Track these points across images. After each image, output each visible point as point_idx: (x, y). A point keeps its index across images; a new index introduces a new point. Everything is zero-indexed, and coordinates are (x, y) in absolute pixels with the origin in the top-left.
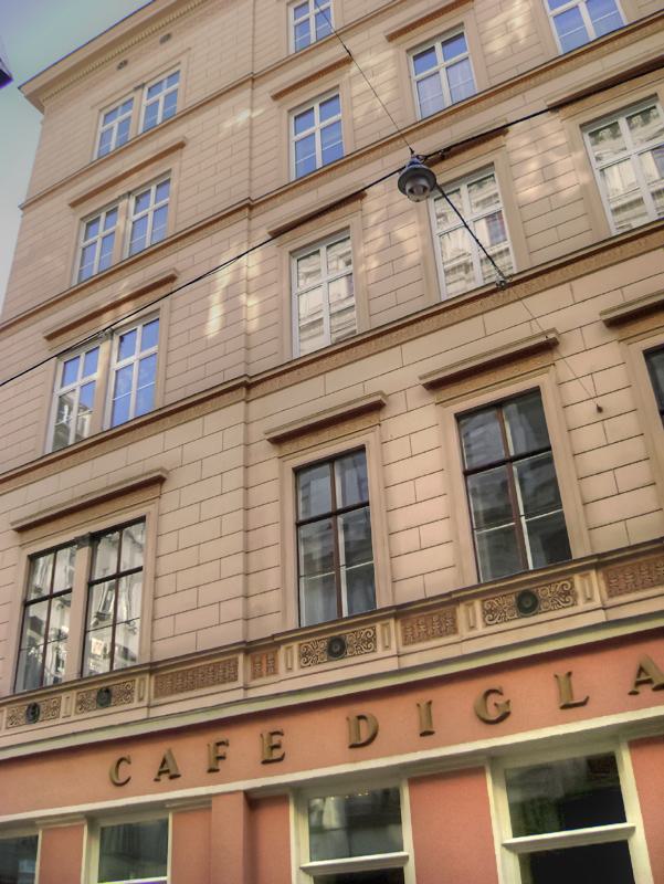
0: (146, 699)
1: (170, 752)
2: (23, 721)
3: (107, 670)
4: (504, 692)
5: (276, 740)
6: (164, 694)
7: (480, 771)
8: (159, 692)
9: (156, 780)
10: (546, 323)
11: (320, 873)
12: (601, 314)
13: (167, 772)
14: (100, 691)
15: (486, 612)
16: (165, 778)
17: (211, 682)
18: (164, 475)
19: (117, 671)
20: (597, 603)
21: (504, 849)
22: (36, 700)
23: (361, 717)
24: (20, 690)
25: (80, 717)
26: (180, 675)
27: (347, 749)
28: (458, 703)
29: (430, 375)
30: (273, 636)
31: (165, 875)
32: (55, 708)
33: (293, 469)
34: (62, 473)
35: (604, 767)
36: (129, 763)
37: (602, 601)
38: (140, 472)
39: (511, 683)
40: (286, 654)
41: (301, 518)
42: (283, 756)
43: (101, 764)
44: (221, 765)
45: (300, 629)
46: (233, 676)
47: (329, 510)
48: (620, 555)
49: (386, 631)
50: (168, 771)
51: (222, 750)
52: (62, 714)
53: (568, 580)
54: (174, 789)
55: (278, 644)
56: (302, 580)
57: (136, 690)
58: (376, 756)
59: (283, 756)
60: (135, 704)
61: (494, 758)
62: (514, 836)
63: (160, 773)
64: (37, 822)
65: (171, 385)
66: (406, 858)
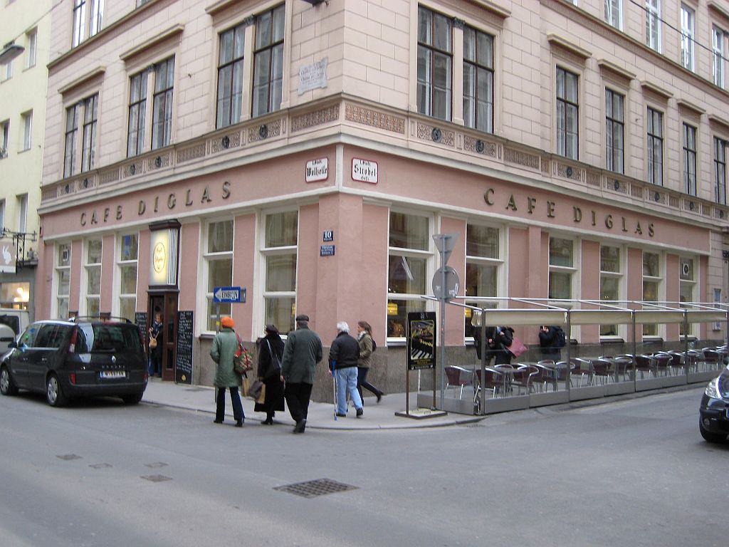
2: (154, 167)
6: (299, 129)
7: (112, 236)
8: (179, 161)
11: (212, 259)
12: (206, 10)
18: (182, 28)
19: (220, 130)
20: (286, 135)
24: (220, 126)
29: (124, 54)
30: (203, 135)
32: (277, 128)
38: (158, 32)
42: (121, 217)
43: (75, 217)
52: (241, 143)
55: (205, 139)
58: (231, 203)
60: (281, 136)
61: (117, 231)
62: (266, 247)
63: (203, 198)
64: (232, 212)
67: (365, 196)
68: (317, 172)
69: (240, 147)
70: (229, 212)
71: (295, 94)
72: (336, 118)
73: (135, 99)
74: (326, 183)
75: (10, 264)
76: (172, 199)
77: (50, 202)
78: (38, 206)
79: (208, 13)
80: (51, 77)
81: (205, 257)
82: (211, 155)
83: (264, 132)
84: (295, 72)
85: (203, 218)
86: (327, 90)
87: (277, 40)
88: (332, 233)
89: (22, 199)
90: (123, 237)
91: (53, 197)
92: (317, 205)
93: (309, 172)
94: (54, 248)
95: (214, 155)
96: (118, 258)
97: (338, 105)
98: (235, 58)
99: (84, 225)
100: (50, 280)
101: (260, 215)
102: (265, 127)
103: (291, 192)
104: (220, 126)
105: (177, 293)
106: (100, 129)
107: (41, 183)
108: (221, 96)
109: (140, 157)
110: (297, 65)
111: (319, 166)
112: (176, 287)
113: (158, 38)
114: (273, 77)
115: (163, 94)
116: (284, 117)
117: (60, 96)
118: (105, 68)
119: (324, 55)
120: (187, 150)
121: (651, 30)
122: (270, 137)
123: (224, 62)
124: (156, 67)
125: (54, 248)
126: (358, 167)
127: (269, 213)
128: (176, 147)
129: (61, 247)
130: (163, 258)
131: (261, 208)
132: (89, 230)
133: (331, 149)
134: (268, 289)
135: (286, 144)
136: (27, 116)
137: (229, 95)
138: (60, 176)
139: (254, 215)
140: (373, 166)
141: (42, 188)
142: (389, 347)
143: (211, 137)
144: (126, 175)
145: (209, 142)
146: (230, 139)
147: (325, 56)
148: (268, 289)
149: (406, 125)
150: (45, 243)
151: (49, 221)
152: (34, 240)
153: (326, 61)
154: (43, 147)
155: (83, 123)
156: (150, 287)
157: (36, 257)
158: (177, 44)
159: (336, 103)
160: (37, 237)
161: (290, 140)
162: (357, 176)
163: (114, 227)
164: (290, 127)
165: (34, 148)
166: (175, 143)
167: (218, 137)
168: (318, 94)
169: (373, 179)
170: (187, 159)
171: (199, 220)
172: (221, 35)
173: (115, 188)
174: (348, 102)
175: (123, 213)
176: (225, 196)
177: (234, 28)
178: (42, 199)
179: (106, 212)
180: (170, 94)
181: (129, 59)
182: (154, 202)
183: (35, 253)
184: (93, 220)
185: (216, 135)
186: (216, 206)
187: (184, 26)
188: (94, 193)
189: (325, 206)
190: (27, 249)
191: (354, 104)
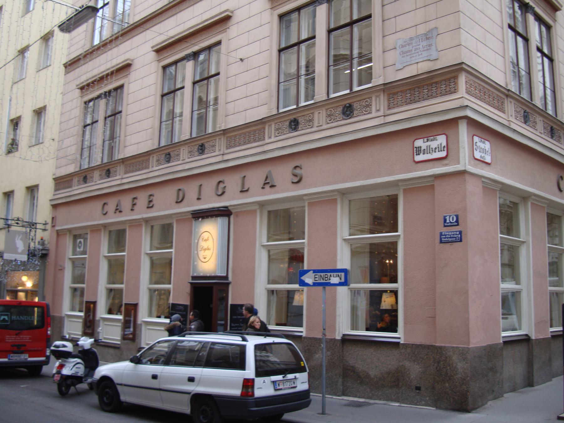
0: (222, 150)
1: (270, 172)
2: (197, 153)
3: (325, 98)
4: (302, 167)
5: (298, 171)
7: (100, 230)
8: (126, 172)
9: (263, 188)
10: (129, 56)
12: (152, 47)
13: (269, 184)
14: (345, 107)
15: (277, 129)
16: (267, 187)
17: (257, 139)
18: (230, 14)
20: (381, 113)
21: (343, 242)
22: (85, 174)
23: (180, 190)
25: (158, 168)
26: (242, 135)
27: (239, 192)
28: (209, 185)
31: (304, 239)
33: (278, 15)
34: (195, 5)
35: (393, 202)
36: (301, 169)
37: (384, 112)
39: (306, 163)
40: (269, 128)
41: (332, 26)
42: (153, 205)
43: (97, 206)
44: (135, 208)
45: (80, 171)
46: (262, 138)
47: (348, 20)
48: (203, 137)
49: (378, 99)
50: (268, 183)
51: (152, 198)
52: (181, 159)
53: (311, 113)
54: (265, 195)
56: (163, 124)
57: (217, 145)
58: (304, 188)
59: (153, 205)
60: (217, 153)
61: (105, 226)
63: (265, 184)
64: (304, 198)
65: (138, 10)
66: (399, 236)
67: (484, 177)
68: (429, 150)
69: (315, 129)
70: (300, 198)
71: (390, 70)
72: (455, 91)
73: (89, 121)
74: (445, 162)
75: (22, 253)
76: (222, 185)
77: (64, 193)
78: (50, 196)
79: (154, 51)
80: (68, 75)
81: (263, 246)
82: (273, 139)
83: (202, 149)
84: (389, 45)
85: (262, 205)
86: (438, 62)
87: (213, 72)
88: (457, 216)
89: (32, 190)
90: (269, 212)
91: (260, 140)
92: (432, 187)
93: (419, 151)
94: (68, 236)
95: (158, 168)
96: (104, 250)
97: (456, 77)
98: (210, 74)
99: (105, 214)
100: (62, 269)
101: (342, 200)
102: (169, 154)
103: (380, 176)
104: (163, 144)
105: (228, 284)
106: (126, 119)
107: (54, 175)
108: (164, 118)
109: (92, 169)
110: (390, 40)
111: (434, 144)
112: (226, 278)
113: (201, 26)
114: (116, 135)
115: (113, 117)
116: (377, 94)
117: (78, 91)
118: (133, 60)
119: (432, 25)
120: (133, 163)
121: (539, 71)
122: (89, 183)
123: (166, 91)
124: (108, 94)
125: (102, 233)
126: (478, 144)
127: (110, 230)
128: (123, 161)
129: (75, 237)
130: (211, 246)
131: (343, 193)
132: (112, 219)
133: (454, 122)
134: (269, 283)
135: (382, 122)
136: (39, 112)
137: (171, 118)
138: (76, 167)
139: (336, 200)
140: (487, 146)
141: (55, 179)
142: (505, 343)
143: (76, 175)
144: (79, 184)
145: (270, 125)
146: (299, 121)
147: (433, 26)
148: (269, 283)
149: (506, 105)
150: (58, 232)
151: (62, 211)
152: (45, 230)
153: (435, 33)
154: (57, 139)
155: (161, 93)
156: (194, 278)
157: (48, 246)
158: (225, 31)
159: (453, 75)
160: (49, 227)
161: (386, 117)
162: (477, 155)
163: (145, 216)
164: (225, 145)
165: (47, 143)
166: (223, 128)
167: (80, 175)
168: (425, 67)
169: (488, 159)
170: (240, 145)
171: (256, 207)
172: (165, 68)
173: (144, 177)
174: (467, 75)
175: (154, 202)
176: (296, 180)
177: (175, 63)
178: (56, 190)
179: (133, 201)
180: (119, 117)
181: (160, 50)
182: (196, 190)
183: (46, 242)
184: (117, 209)
185: (79, 174)
186: (283, 191)
187: (232, 12)
188: (118, 182)
189: (441, 188)
190: (38, 239)
191: (471, 77)
